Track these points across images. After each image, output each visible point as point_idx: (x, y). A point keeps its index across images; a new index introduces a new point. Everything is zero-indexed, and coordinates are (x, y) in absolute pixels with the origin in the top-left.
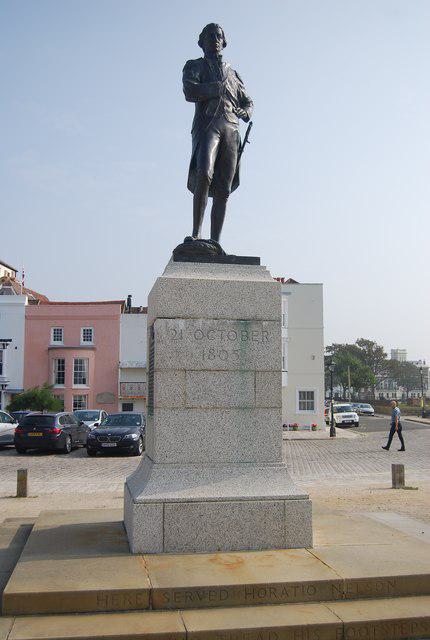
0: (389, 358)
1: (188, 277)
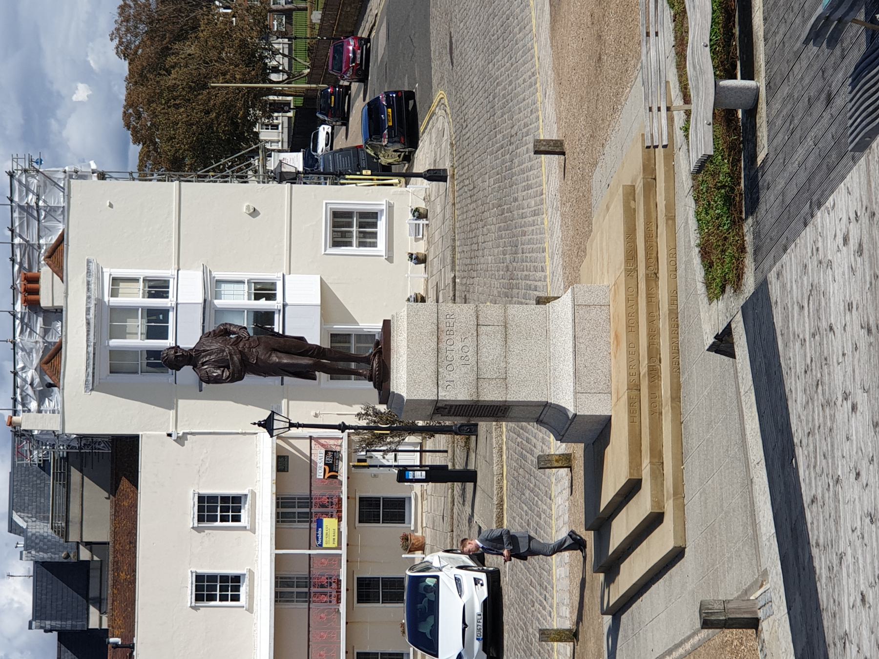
1: (405, 376)
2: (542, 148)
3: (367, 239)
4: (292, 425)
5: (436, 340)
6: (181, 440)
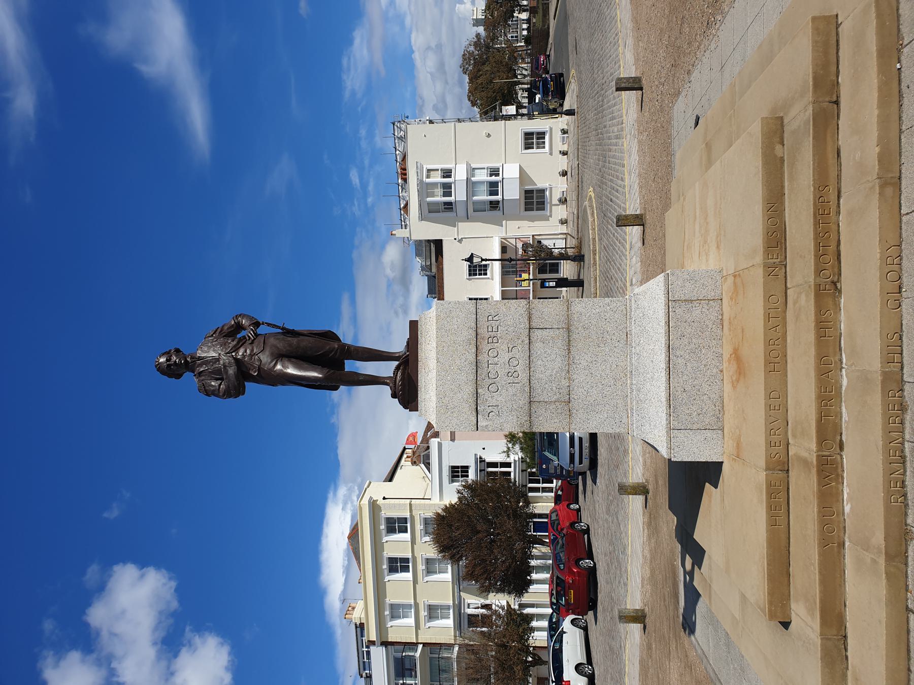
0: (481, 30)
1: (434, 399)
2: (623, 85)
3: (541, 145)
4: (483, 260)
5: (474, 350)
6: (460, 241)
